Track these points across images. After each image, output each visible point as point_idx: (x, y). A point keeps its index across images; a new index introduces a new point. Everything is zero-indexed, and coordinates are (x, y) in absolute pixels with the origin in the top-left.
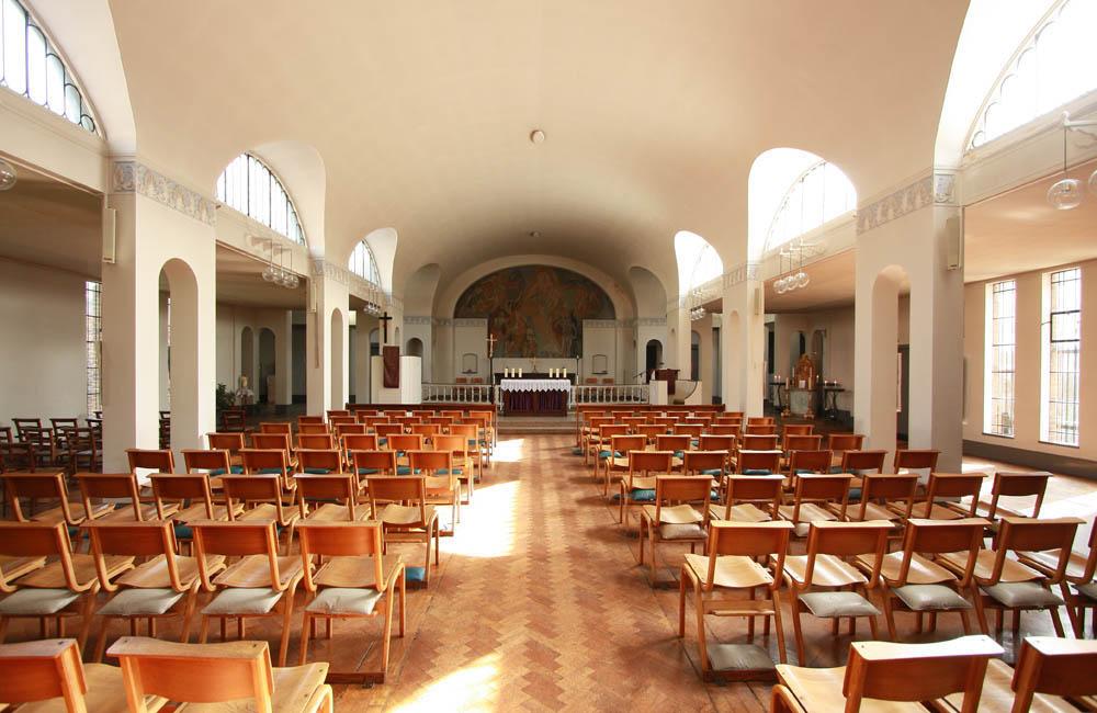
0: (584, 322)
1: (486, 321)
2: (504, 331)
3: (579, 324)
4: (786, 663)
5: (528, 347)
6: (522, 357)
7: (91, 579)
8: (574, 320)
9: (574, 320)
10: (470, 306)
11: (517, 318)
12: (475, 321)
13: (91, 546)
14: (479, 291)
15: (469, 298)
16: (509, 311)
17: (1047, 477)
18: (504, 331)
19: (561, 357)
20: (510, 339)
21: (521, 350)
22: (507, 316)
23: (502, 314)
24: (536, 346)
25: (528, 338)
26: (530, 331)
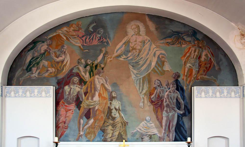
0: (195, 89)
1: (51, 90)
2: (78, 103)
3: (186, 94)
4: (48, 75)
5: (114, 126)
6: (105, 140)
7: (167, 55)
8: (179, 88)
9: (179, 88)
10: (29, 69)
11: (98, 86)
12: (36, 89)
13: (57, 124)
14: (43, 47)
15: (29, 59)
16: (86, 76)
17: (110, 119)
18: (78, 103)
19: (161, 139)
20: (88, 115)
21: (103, 131)
22: (82, 82)
23: (76, 79)
24: (125, 124)
25: (115, 113)
26: (116, 104)
